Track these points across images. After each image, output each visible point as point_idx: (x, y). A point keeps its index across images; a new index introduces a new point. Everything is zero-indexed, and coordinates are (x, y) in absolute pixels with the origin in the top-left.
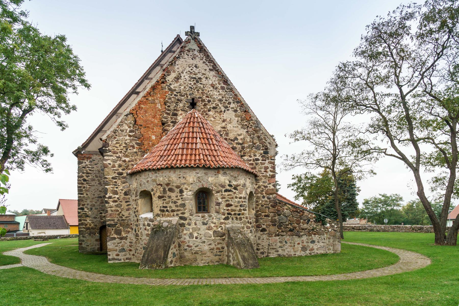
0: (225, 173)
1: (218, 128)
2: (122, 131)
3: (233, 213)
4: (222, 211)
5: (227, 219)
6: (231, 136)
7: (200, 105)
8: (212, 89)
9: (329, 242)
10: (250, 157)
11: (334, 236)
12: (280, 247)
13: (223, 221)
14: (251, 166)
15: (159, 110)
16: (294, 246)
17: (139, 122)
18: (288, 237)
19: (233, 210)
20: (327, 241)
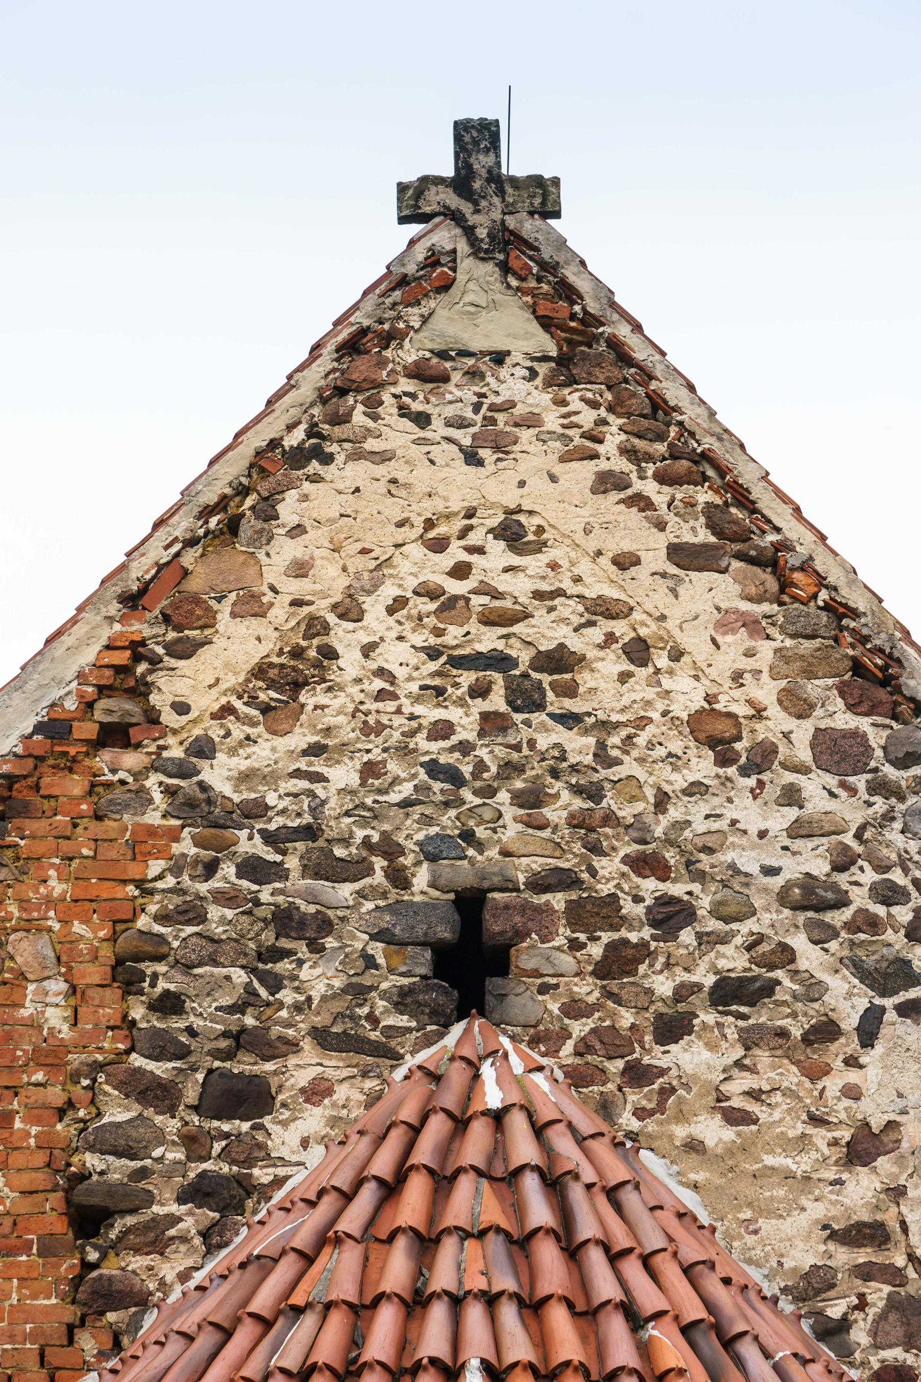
8: (703, 766)
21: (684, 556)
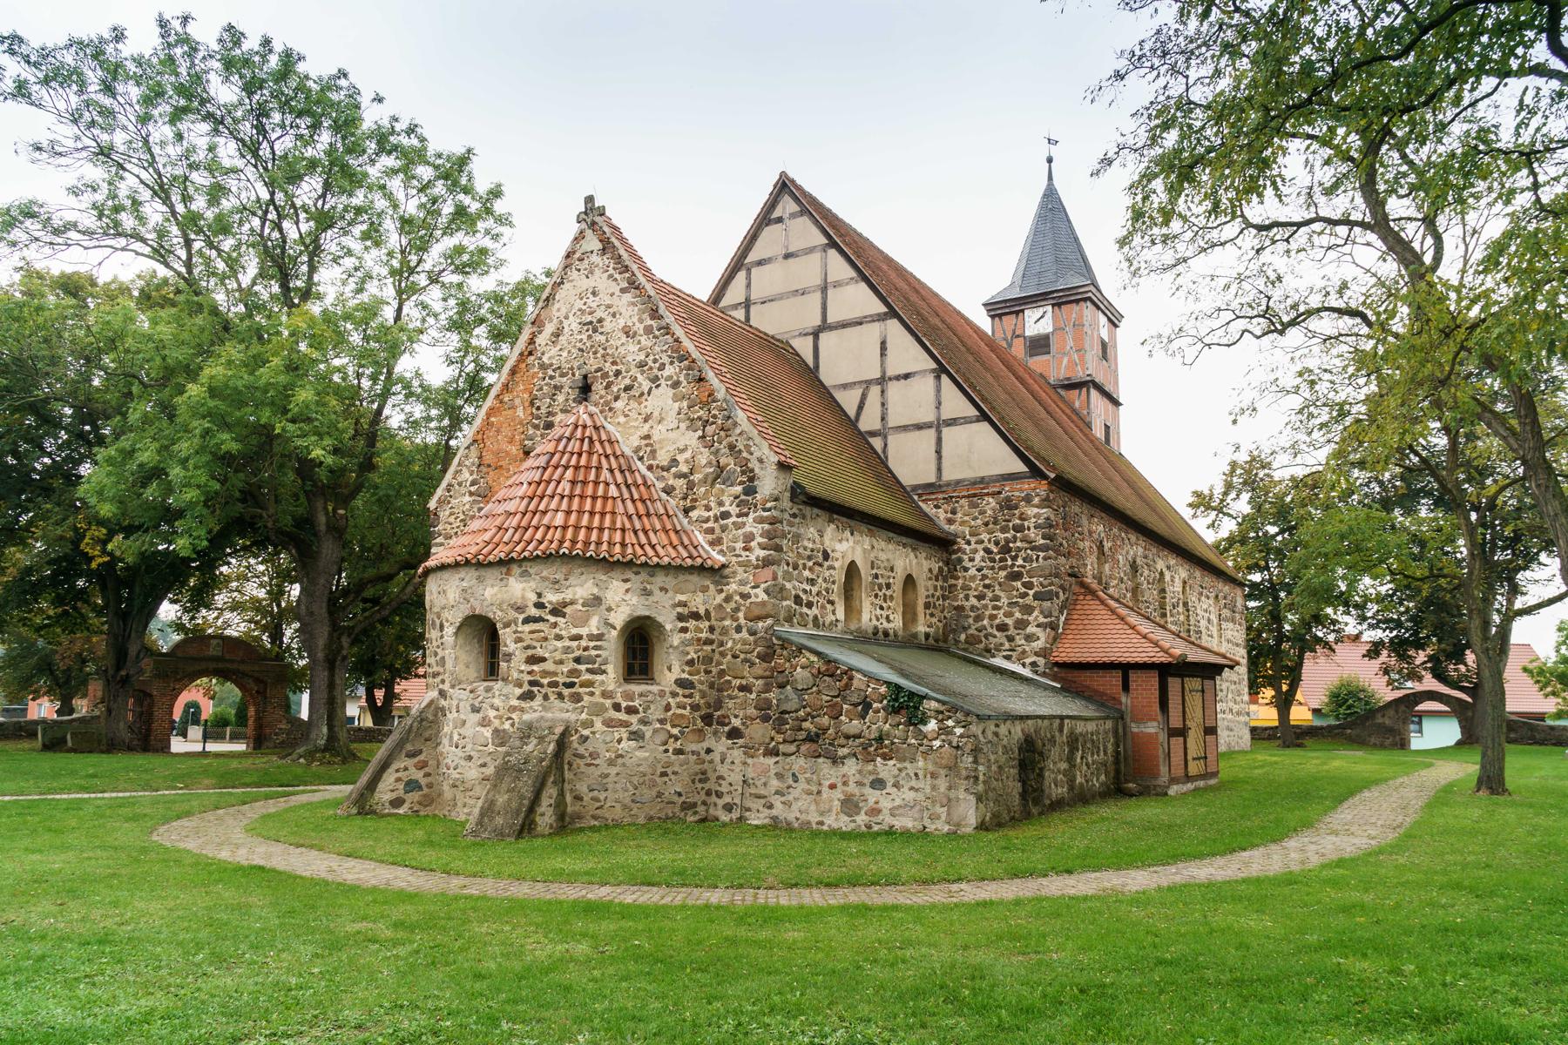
0: (525, 574)
1: (635, 441)
2: (460, 484)
3: (545, 681)
4: (515, 675)
5: (528, 696)
6: (663, 458)
7: (598, 387)
8: (624, 339)
9: (934, 788)
10: (708, 508)
11: (952, 768)
12: (777, 793)
13: (515, 703)
14: (710, 537)
15: (521, 423)
16: (819, 792)
17: (488, 458)
18: (801, 761)
19: (545, 673)
20: (925, 785)
21: (623, 291)
